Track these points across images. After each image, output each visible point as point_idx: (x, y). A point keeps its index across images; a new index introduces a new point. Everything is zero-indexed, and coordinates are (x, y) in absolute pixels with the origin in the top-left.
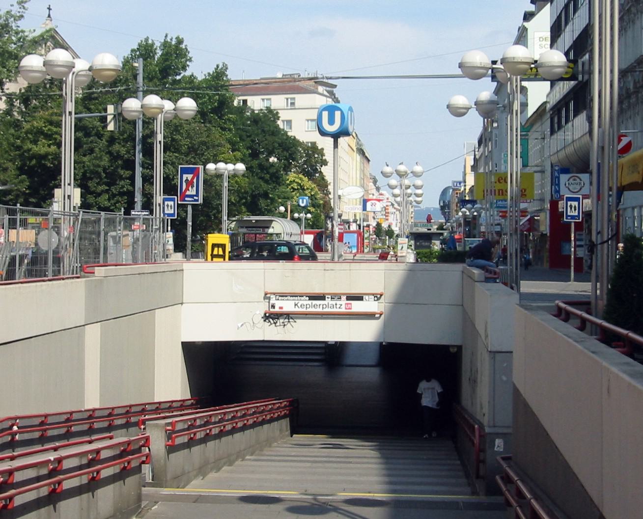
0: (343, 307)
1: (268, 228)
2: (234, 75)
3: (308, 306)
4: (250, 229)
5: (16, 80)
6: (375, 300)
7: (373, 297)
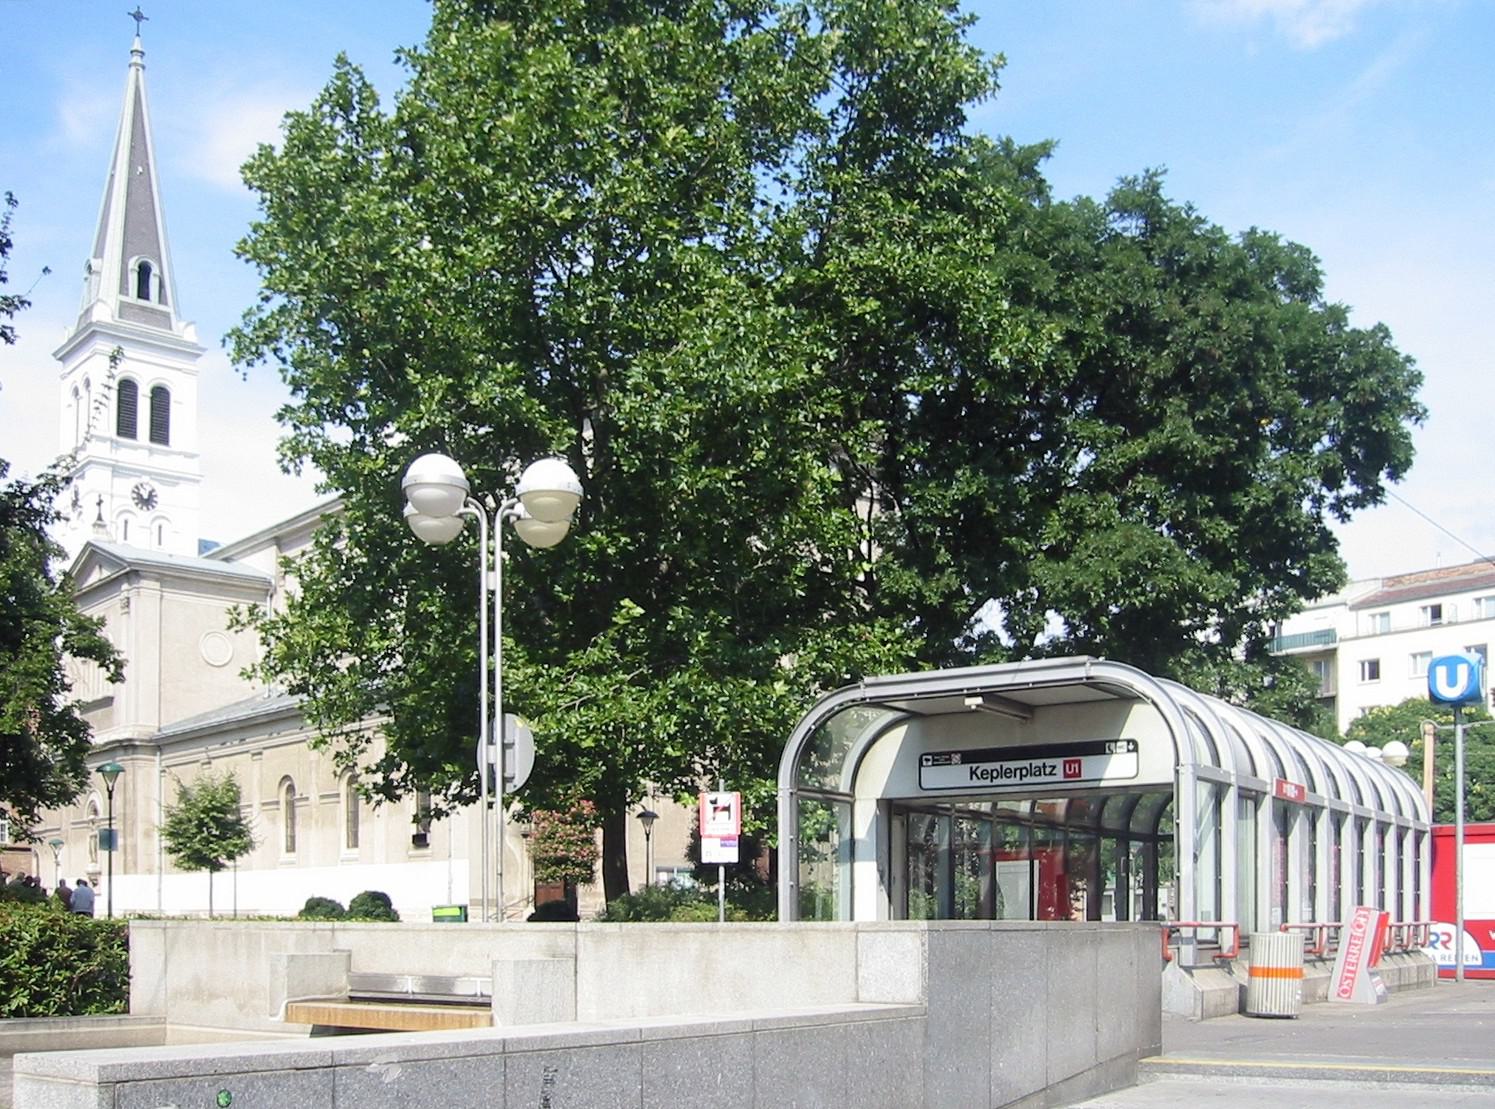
0: (1059, 771)
1: (1099, 749)
2: (879, 797)
3: (995, 774)
4: (989, 766)
5: (1363, 710)
6: (1129, 751)
7: (1125, 743)
